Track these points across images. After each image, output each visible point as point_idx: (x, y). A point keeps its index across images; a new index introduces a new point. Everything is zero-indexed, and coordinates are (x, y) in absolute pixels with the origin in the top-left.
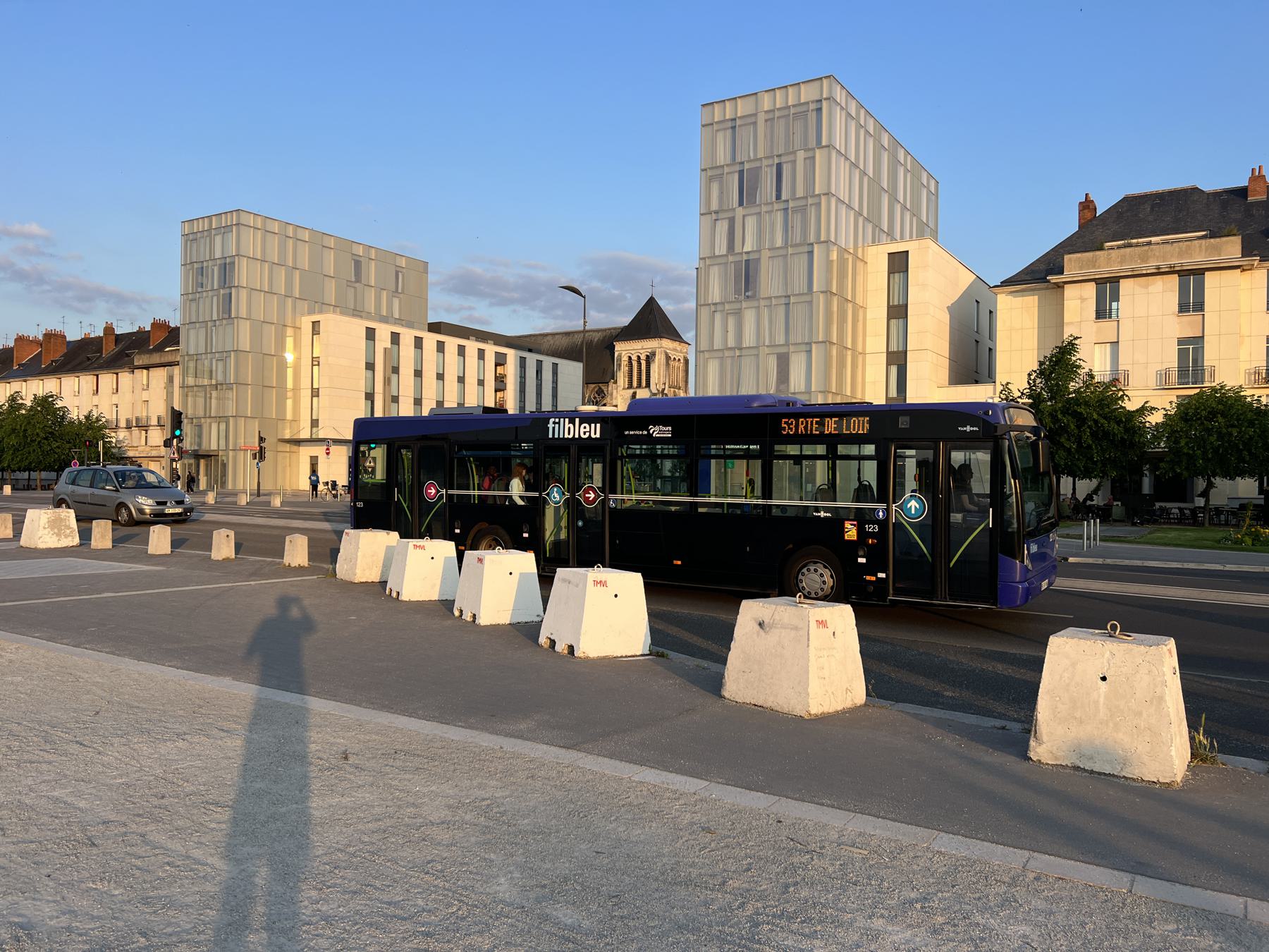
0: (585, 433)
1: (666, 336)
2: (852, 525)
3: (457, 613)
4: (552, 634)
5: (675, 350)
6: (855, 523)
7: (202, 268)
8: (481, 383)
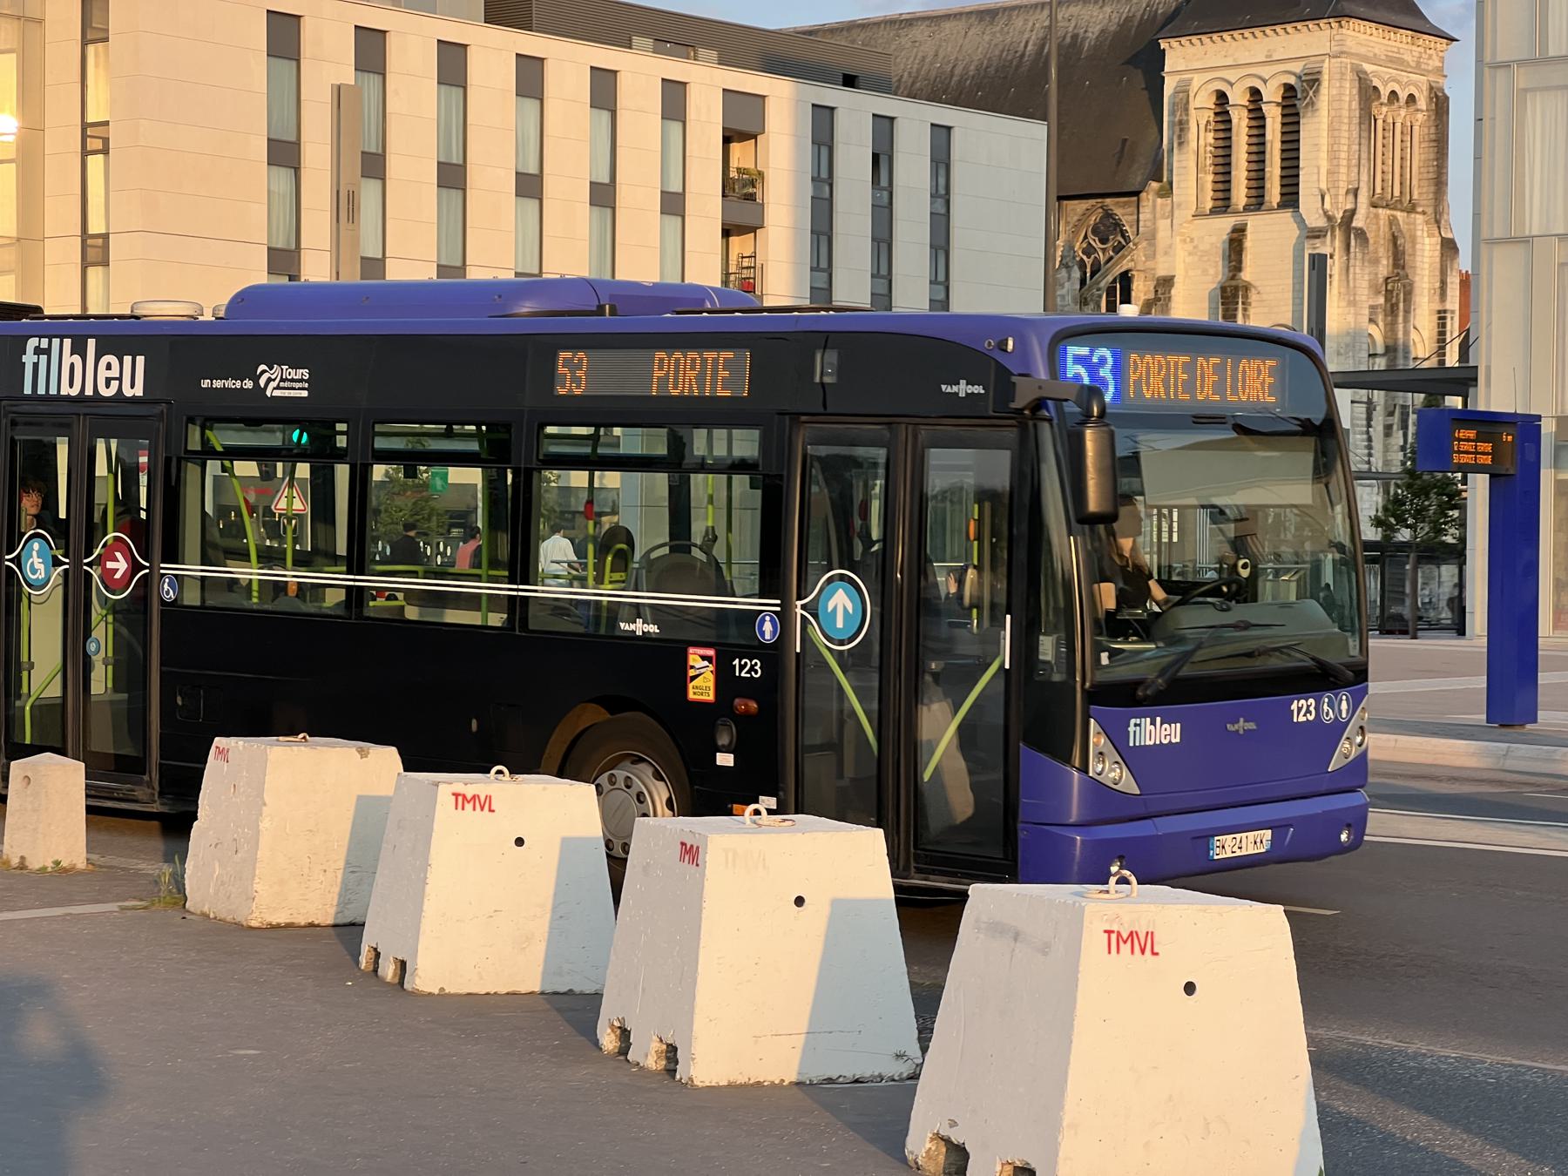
0: (108, 381)
1: (1362, 10)
2: (704, 658)
3: (609, 1041)
4: (953, 1124)
5: (1396, 62)
6: (711, 652)
8: (673, 204)
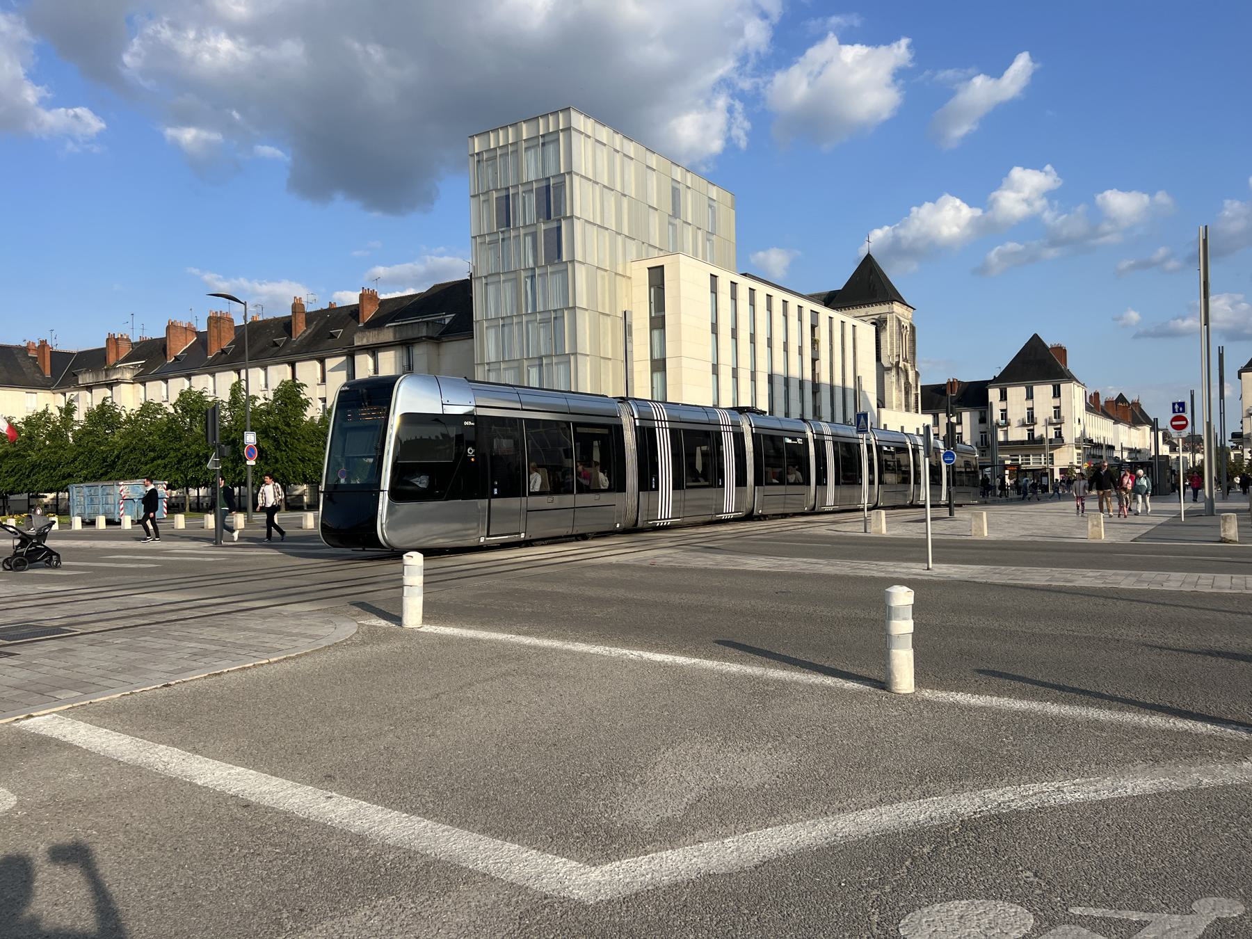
7: (507, 197)
